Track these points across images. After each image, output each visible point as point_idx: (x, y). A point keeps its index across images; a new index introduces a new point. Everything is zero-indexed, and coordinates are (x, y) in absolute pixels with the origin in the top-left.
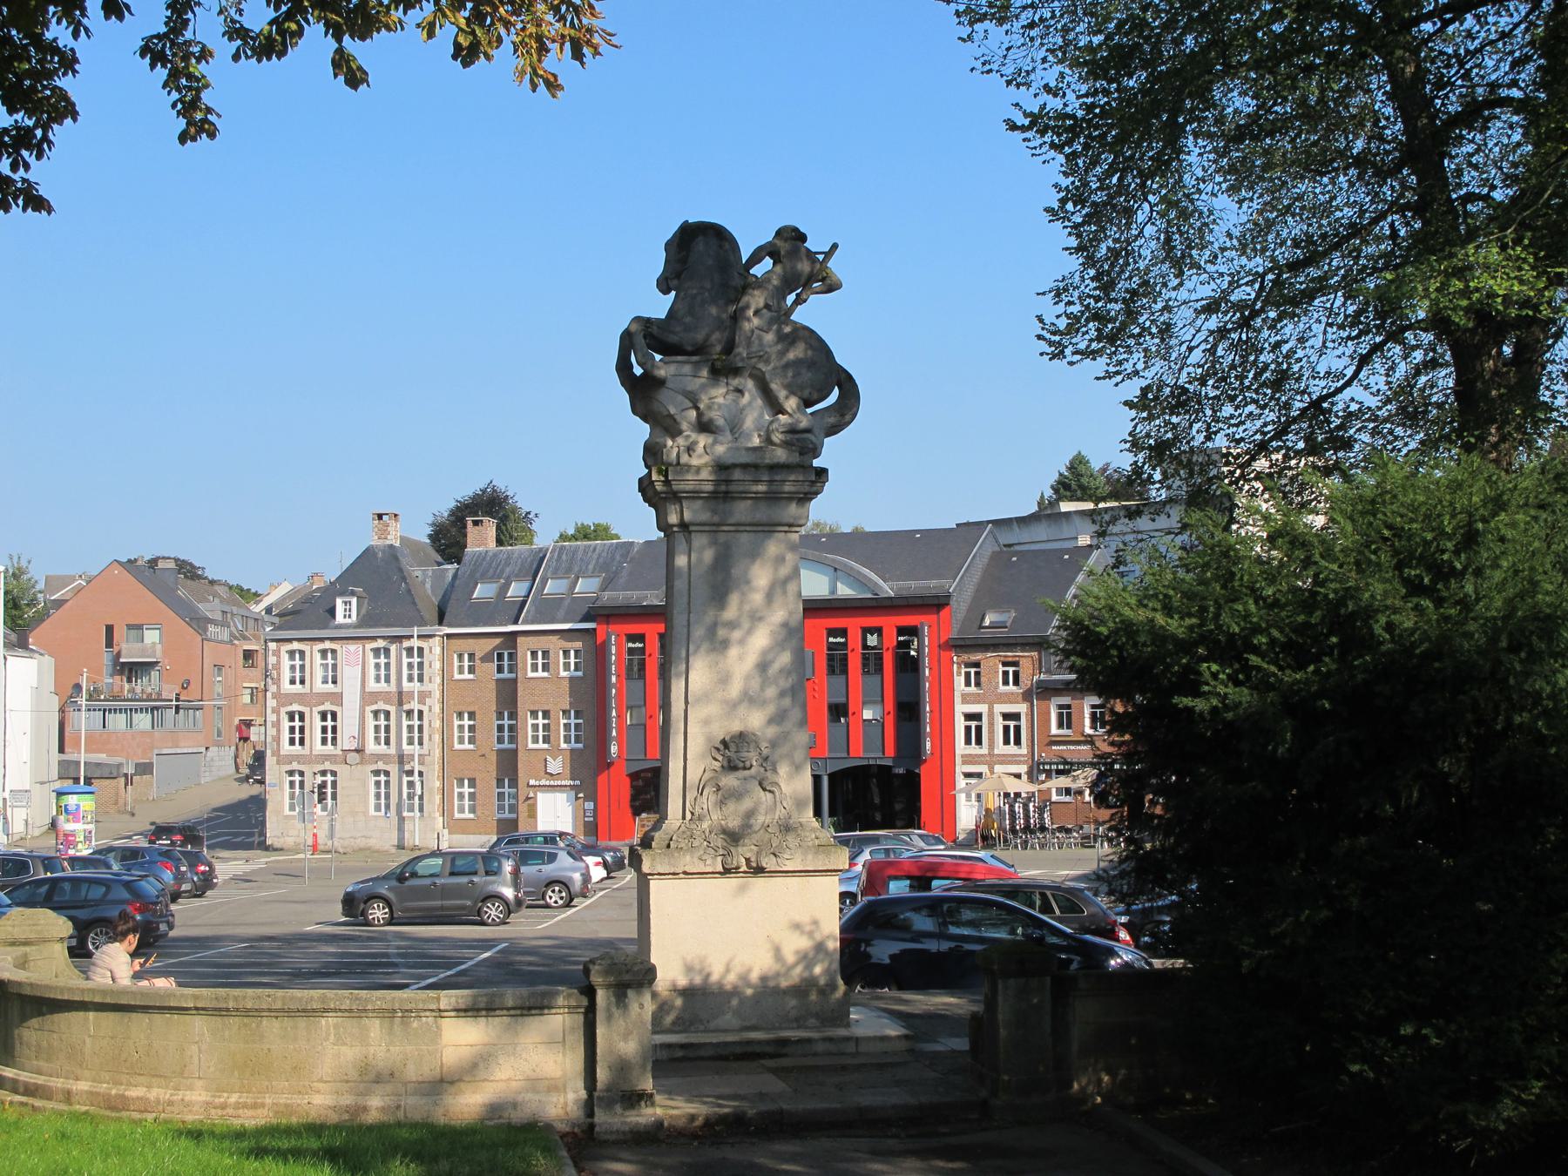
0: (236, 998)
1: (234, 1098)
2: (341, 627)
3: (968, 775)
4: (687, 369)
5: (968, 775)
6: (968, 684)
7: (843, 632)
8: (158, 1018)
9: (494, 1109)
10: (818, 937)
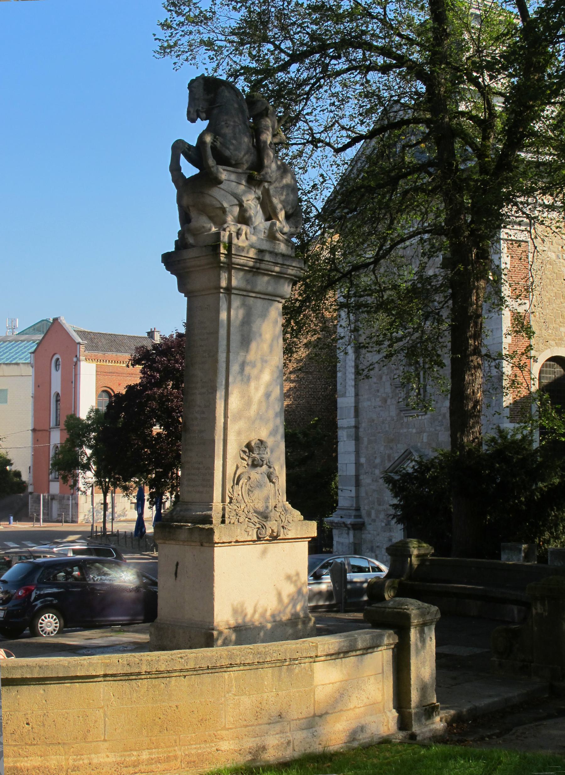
0: (149, 663)
1: (145, 756)
4: (233, 177)
8: (54, 689)
9: (353, 735)
10: (299, 584)
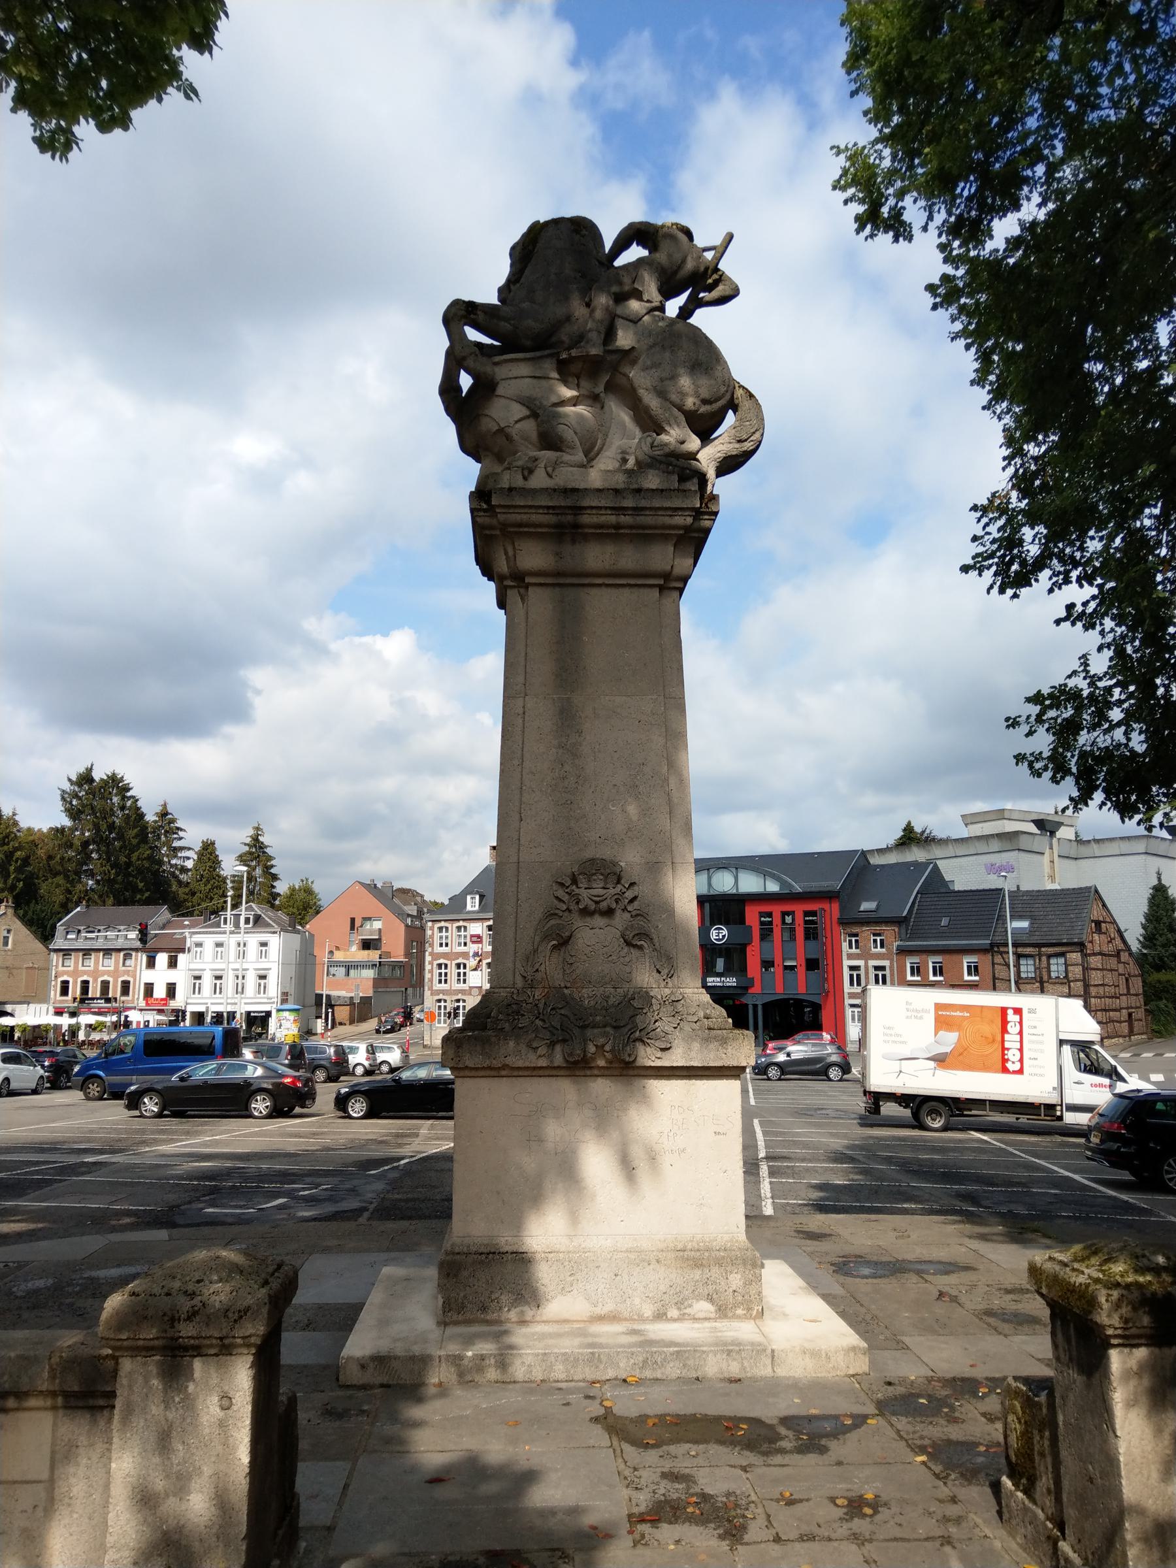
2: (470, 912)
3: (852, 1006)
5: (852, 1006)
6: (851, 947)
7: (770, 915)
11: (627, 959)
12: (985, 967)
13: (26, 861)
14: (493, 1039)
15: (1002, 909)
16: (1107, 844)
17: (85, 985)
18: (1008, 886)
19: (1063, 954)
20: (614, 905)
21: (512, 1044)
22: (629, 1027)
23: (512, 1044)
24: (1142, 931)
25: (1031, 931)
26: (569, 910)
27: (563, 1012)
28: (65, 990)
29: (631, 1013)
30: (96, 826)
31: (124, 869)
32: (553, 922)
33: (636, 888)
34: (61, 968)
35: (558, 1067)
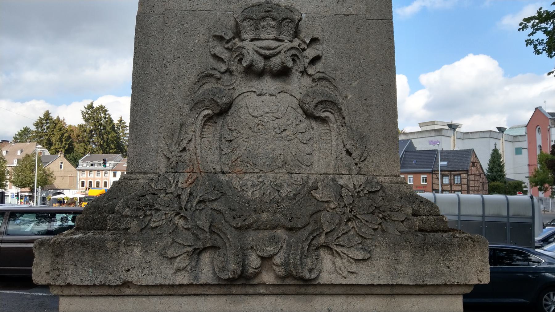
11: (307, 136)
12: (430, 179)
13: (69, 137)
14: (110, 245)
15: (437, 157)
16: (475, 134)
17: (90, 183)
18: (439, 149)
19: (460, 175)
20: (290, 64)
21: (137, 252)
22: (310, 228)
23: (137, 252)
24: (488, 166)
25: (448, 166)
26: (229, 71)
27: (215, 205)
28: (83, 185)
29: (313, 209)
30: (95, 125)
31: (107, 141)
32: (207, 87)
33: (319, 46)
34: (81, 177)
35: (206, 285)
